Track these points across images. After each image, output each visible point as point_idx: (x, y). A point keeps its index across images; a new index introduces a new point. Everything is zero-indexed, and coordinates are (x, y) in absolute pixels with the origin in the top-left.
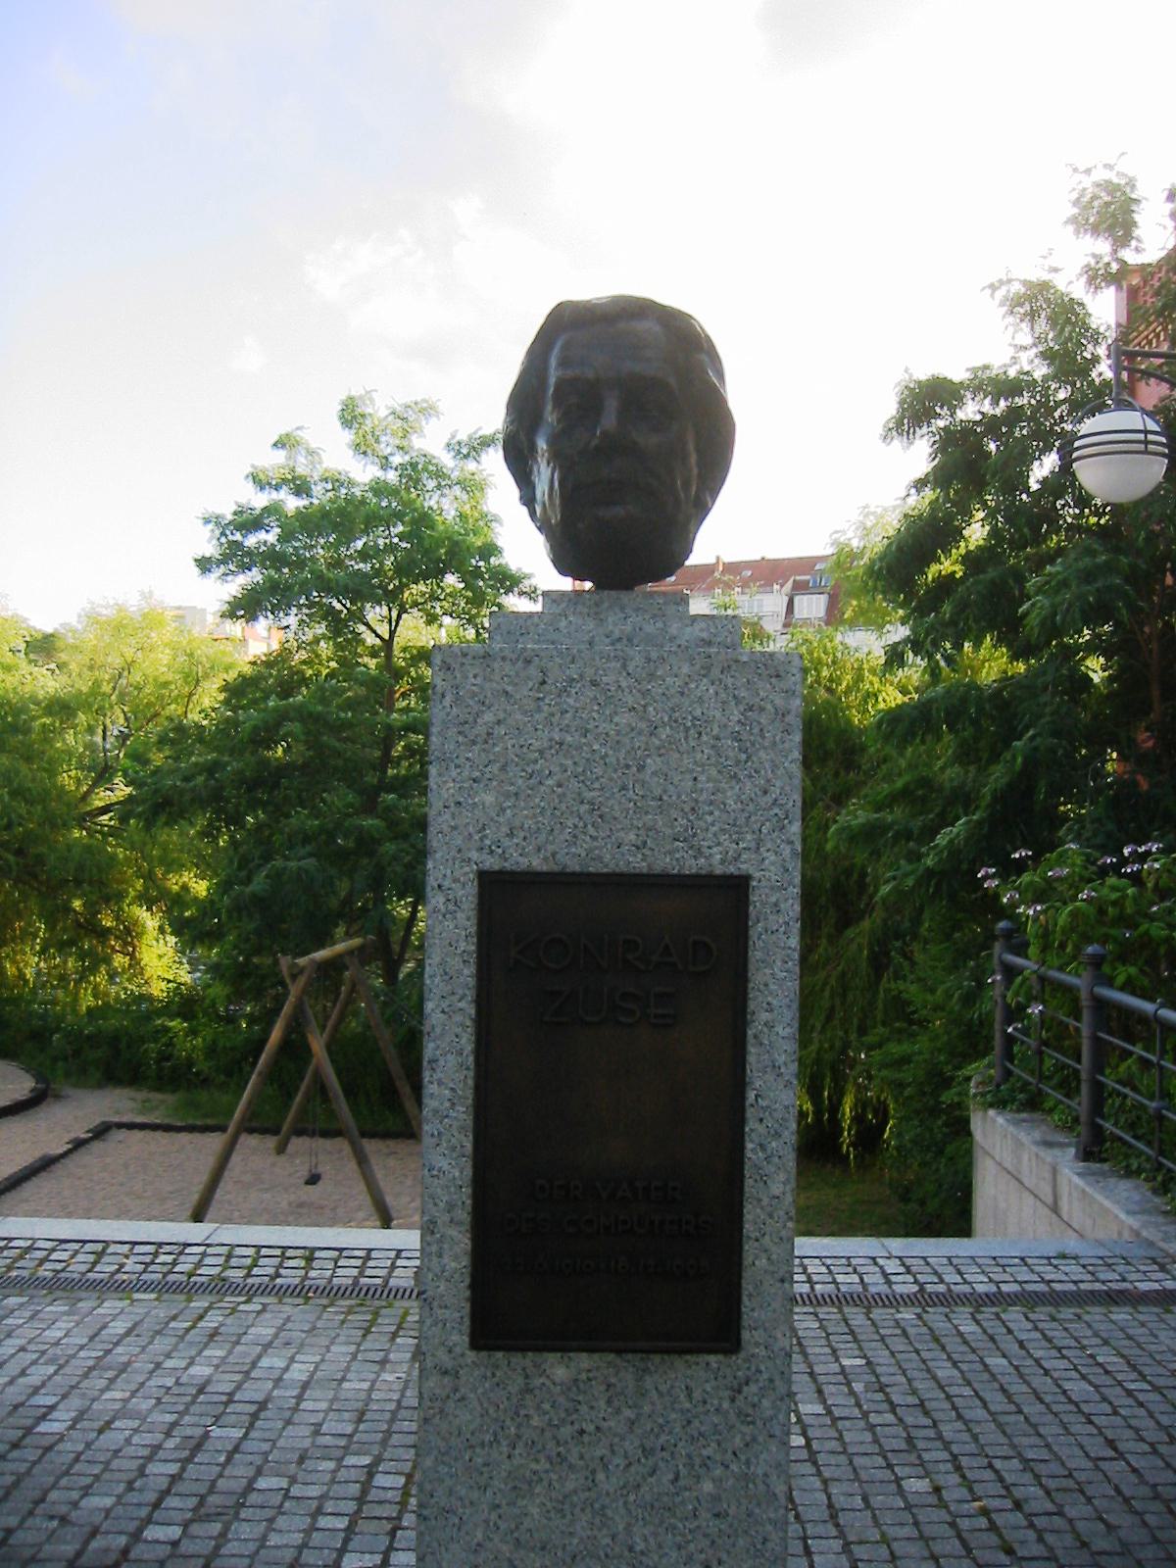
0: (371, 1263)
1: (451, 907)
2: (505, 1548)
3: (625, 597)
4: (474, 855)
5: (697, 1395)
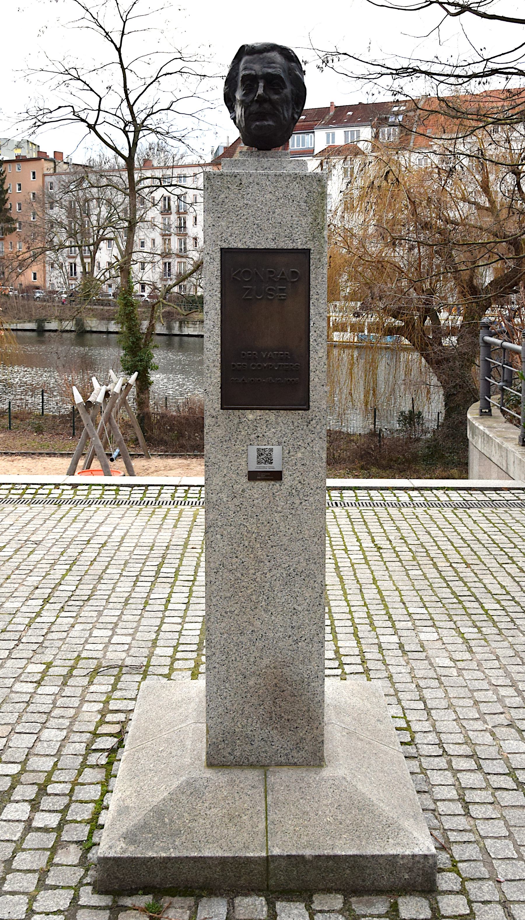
0: (148, 492)
1: (212, 261)
2: (234, 476)
3: (268, 153)
4: (219, 243)
5: (296, 424)
